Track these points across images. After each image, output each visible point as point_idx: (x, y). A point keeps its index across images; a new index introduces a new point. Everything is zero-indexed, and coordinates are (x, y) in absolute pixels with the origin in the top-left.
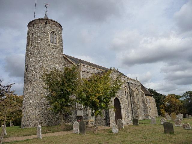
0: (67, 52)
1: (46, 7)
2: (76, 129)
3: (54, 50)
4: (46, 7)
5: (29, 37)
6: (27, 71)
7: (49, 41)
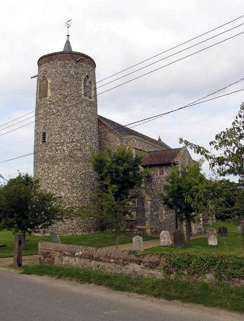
0: (101, 112)
1: (68, 27)
2: (166, 240)
3: (89, 108)
4: (68, 27)
5: (47, 81)
6: (44, 141)
7: (83, 92)
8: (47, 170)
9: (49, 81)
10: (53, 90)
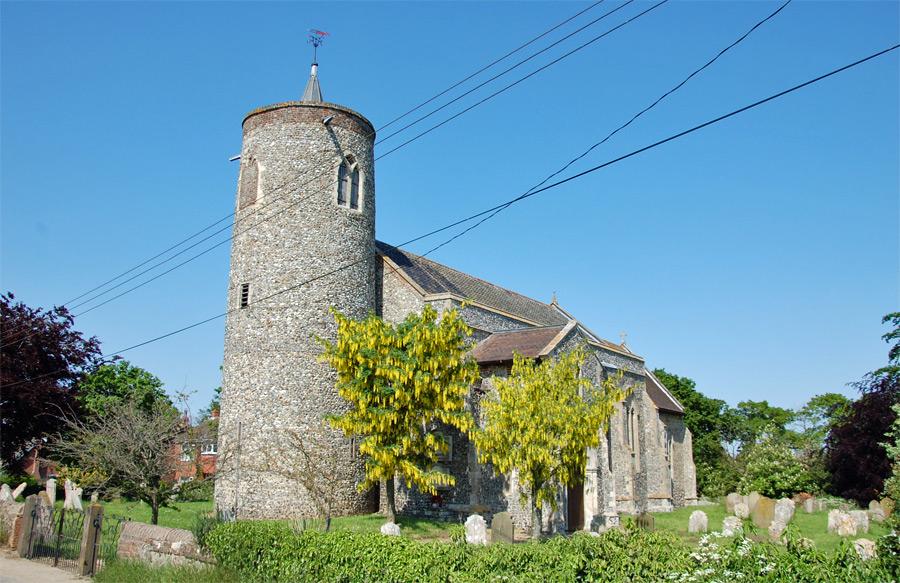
1: (316, 46)
5: (257, 170)
8: (247, 369)
9: (262, 168)
10: (269, 190)
